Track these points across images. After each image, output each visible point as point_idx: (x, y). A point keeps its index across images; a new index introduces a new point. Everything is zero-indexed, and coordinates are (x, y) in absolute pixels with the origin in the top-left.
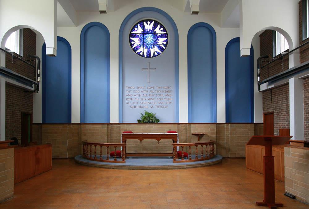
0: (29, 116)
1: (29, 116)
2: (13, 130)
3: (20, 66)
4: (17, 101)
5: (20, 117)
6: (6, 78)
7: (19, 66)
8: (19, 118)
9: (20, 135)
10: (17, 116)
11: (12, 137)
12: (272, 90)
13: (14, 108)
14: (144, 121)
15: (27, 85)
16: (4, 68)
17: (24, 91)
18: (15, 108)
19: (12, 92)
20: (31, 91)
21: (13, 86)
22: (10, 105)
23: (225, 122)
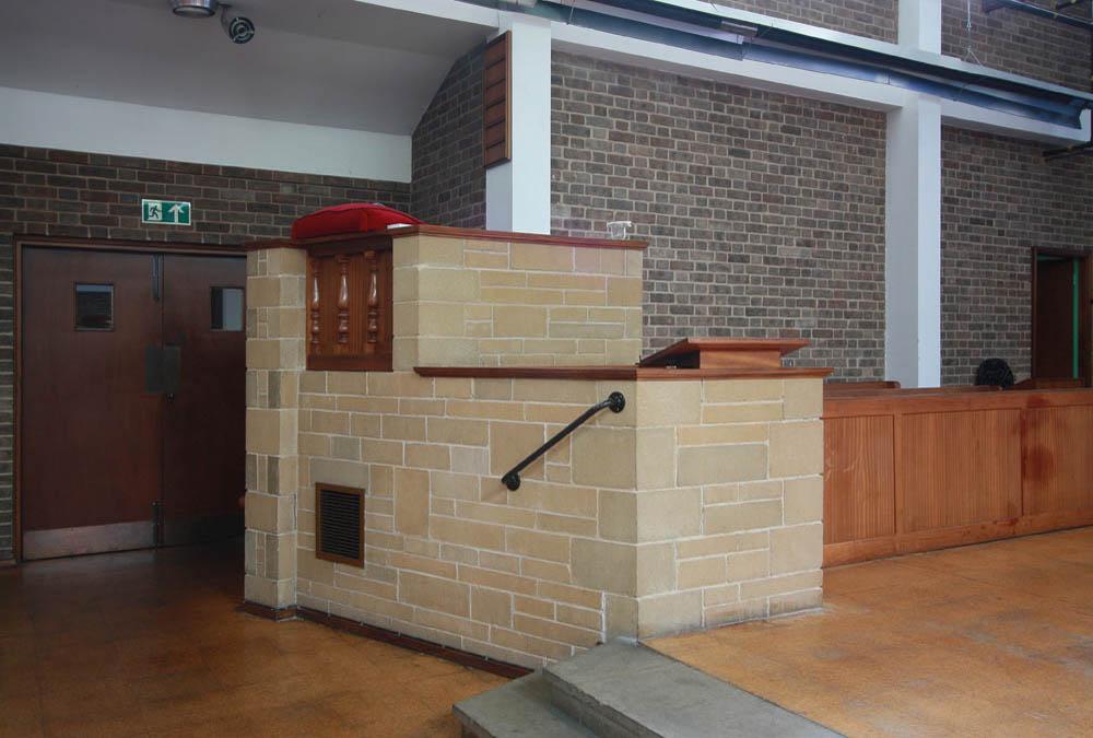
0: (1076, 265)
1: (1076, 265)
2: (988, 326)
3: (1025, 41)
4: (1009, 200)
5: (1024, 269)
6: (943, 100)
7: (1018, 39)
8: (1022, 277)
9: (1023, 352)
10: (1012, 268)
11: (986, 358)
12: (519, 473)
13: (994, 231)
14: (790, 251)
15: (1053, 117)
16: (934, 54)
17: (1045, 154)
18: (1001, 233)
19: (986, 161)
20: (1075, 148)
21: (990, 136)
22: (977, 222)
23: (395, 241)
